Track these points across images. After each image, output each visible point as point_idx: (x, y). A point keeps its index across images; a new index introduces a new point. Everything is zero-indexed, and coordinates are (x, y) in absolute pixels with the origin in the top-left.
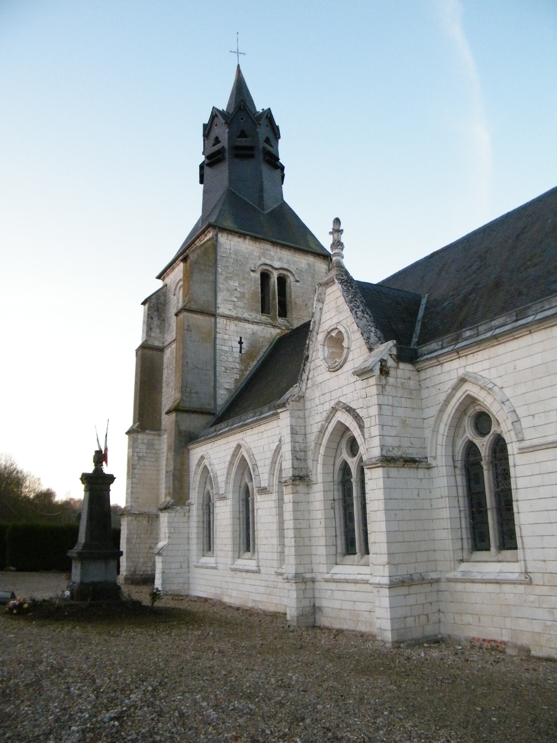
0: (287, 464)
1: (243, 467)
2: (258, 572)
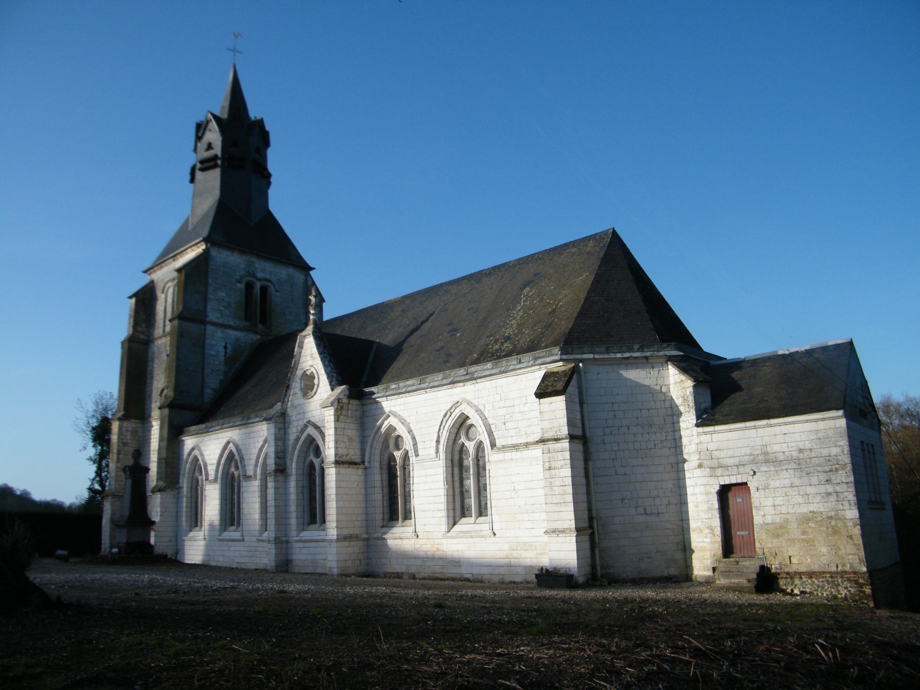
0: (271, 462)
1: (232, 459)
2: (243, 540)
